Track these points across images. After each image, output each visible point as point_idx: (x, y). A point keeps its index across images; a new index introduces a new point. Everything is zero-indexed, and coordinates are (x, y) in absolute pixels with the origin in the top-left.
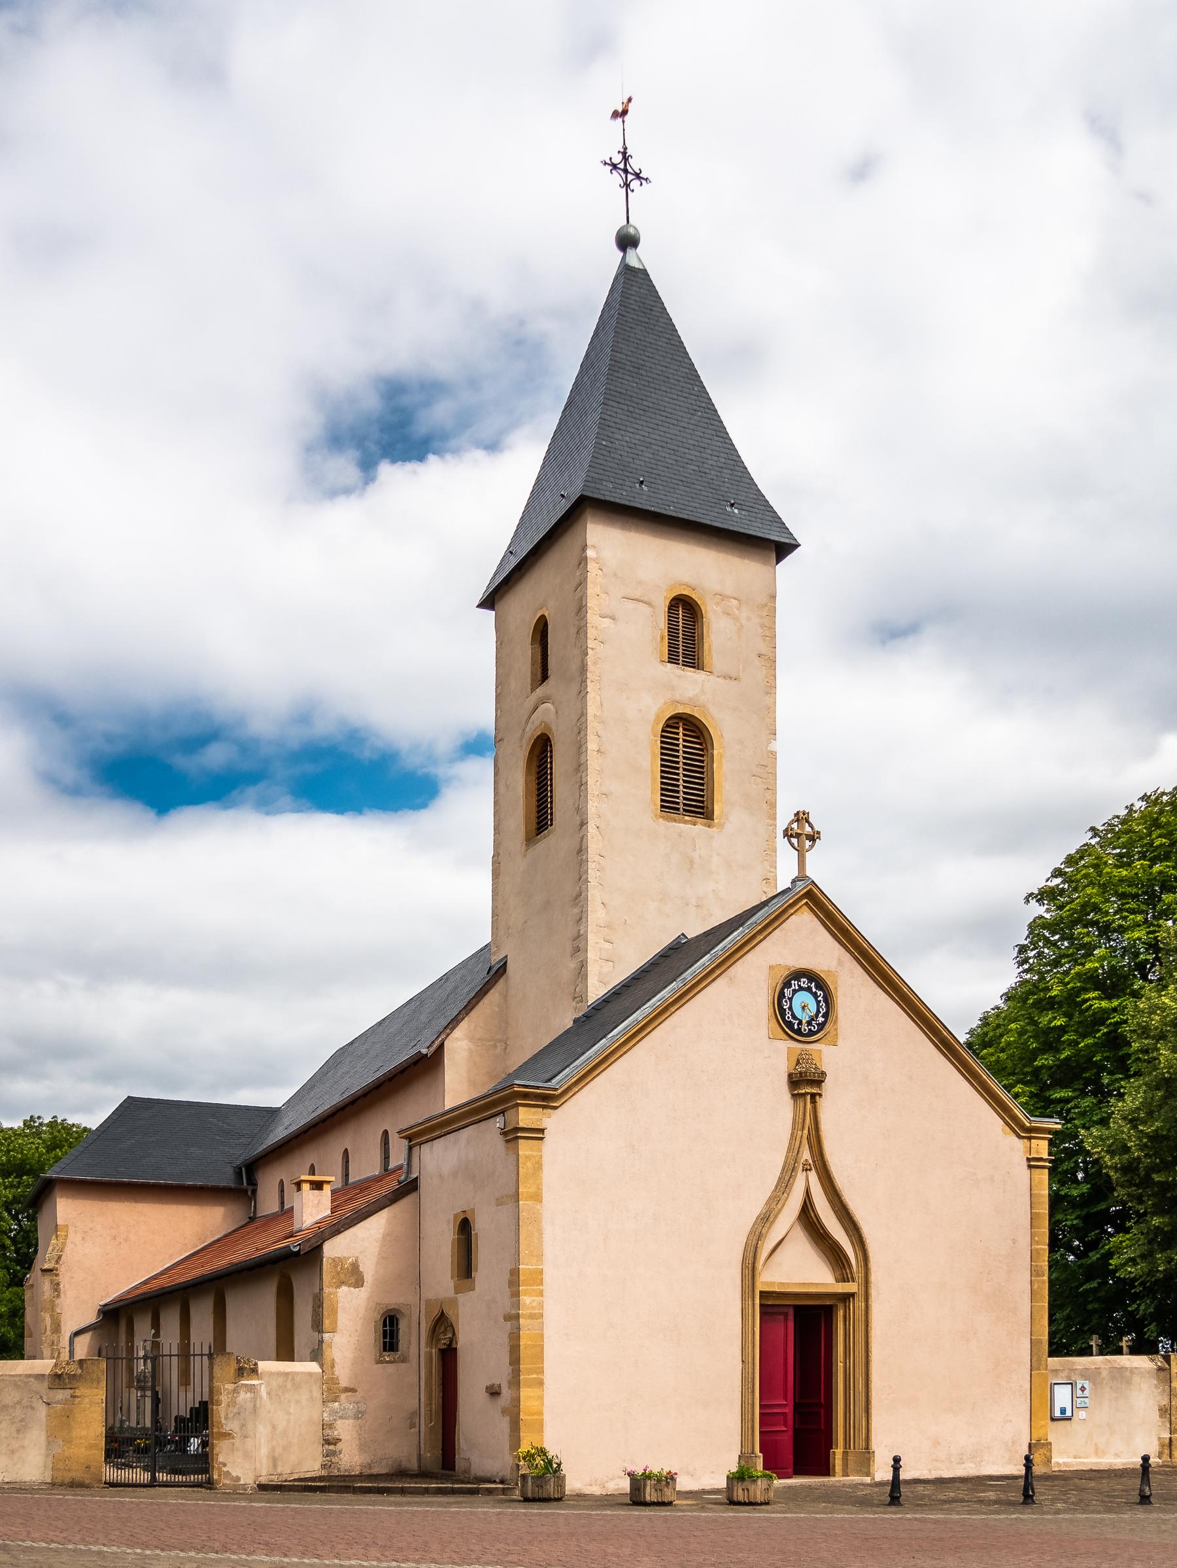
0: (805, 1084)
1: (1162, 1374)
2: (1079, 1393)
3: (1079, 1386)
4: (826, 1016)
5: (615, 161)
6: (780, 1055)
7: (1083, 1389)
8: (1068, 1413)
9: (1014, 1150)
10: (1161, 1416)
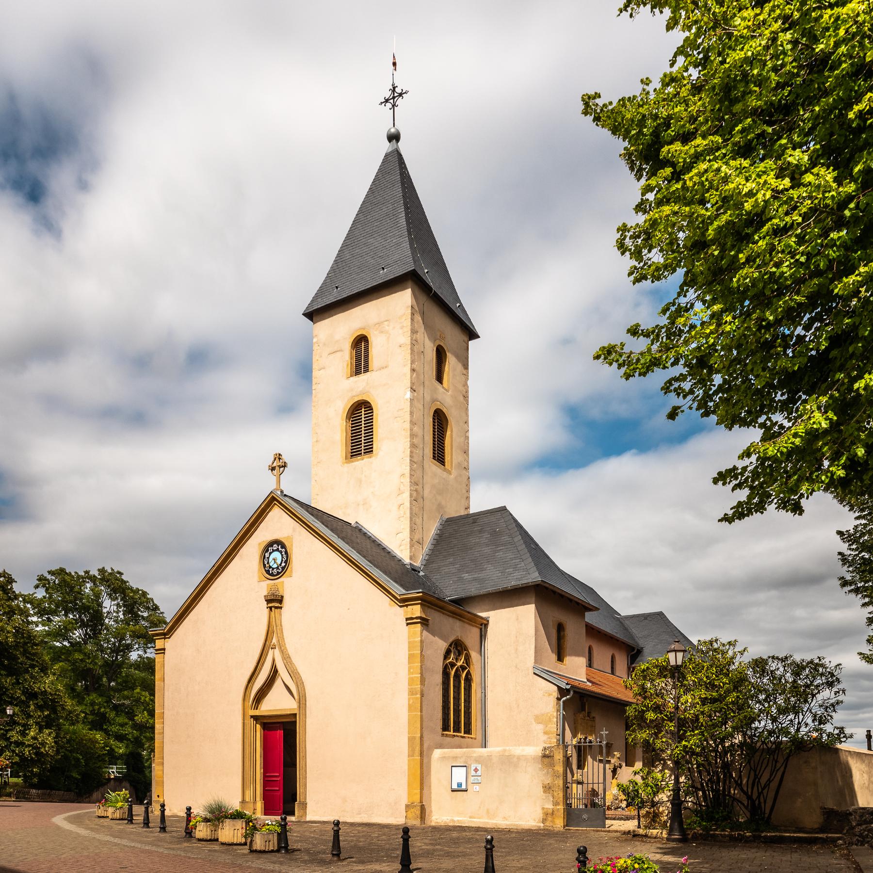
0: (275, 601)
1: (547, 760)
2: (473, 773)
3: (473, 768)
4: (286, 562)
5: (396, 89)
6: (264, 587)
7: (476, 770)
8: (464, 787)
9: (399, 614)
10: (545, 792)
